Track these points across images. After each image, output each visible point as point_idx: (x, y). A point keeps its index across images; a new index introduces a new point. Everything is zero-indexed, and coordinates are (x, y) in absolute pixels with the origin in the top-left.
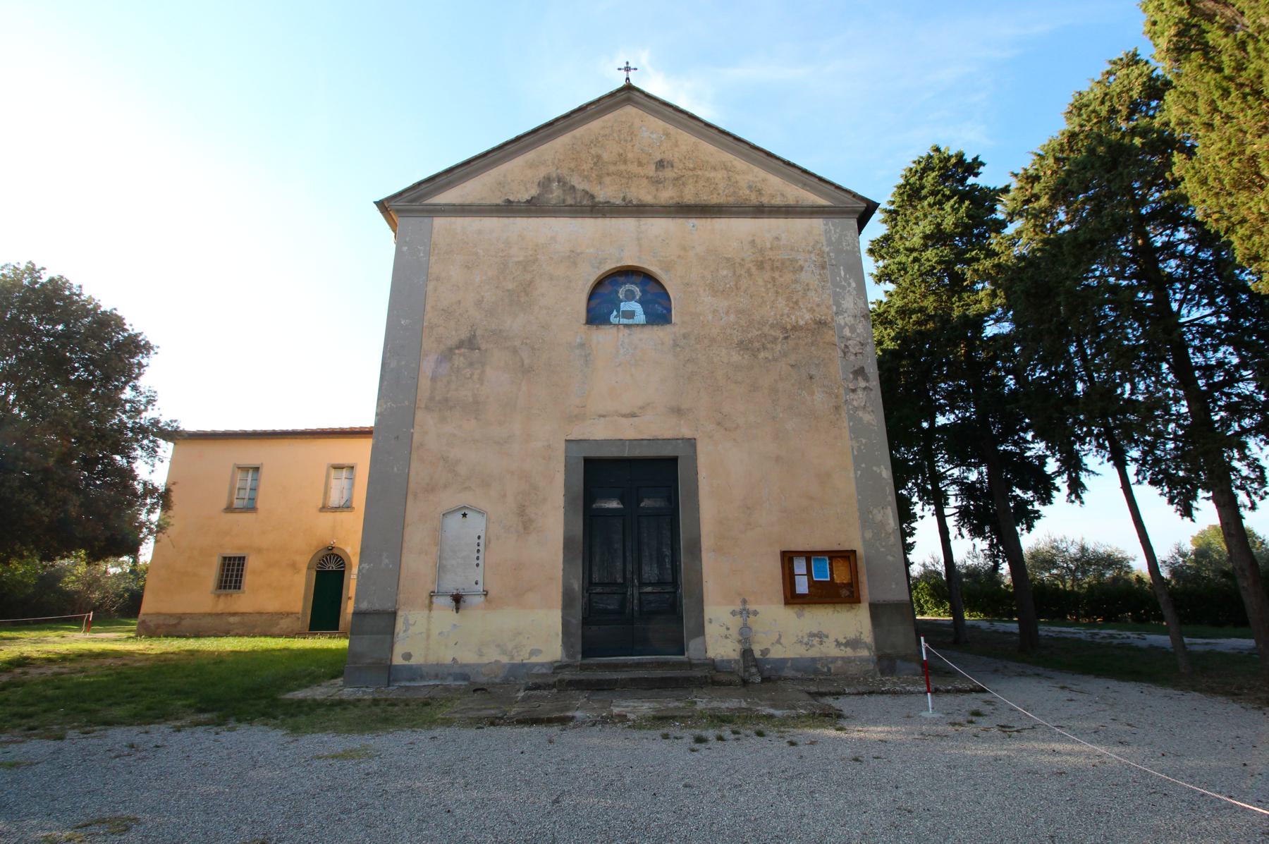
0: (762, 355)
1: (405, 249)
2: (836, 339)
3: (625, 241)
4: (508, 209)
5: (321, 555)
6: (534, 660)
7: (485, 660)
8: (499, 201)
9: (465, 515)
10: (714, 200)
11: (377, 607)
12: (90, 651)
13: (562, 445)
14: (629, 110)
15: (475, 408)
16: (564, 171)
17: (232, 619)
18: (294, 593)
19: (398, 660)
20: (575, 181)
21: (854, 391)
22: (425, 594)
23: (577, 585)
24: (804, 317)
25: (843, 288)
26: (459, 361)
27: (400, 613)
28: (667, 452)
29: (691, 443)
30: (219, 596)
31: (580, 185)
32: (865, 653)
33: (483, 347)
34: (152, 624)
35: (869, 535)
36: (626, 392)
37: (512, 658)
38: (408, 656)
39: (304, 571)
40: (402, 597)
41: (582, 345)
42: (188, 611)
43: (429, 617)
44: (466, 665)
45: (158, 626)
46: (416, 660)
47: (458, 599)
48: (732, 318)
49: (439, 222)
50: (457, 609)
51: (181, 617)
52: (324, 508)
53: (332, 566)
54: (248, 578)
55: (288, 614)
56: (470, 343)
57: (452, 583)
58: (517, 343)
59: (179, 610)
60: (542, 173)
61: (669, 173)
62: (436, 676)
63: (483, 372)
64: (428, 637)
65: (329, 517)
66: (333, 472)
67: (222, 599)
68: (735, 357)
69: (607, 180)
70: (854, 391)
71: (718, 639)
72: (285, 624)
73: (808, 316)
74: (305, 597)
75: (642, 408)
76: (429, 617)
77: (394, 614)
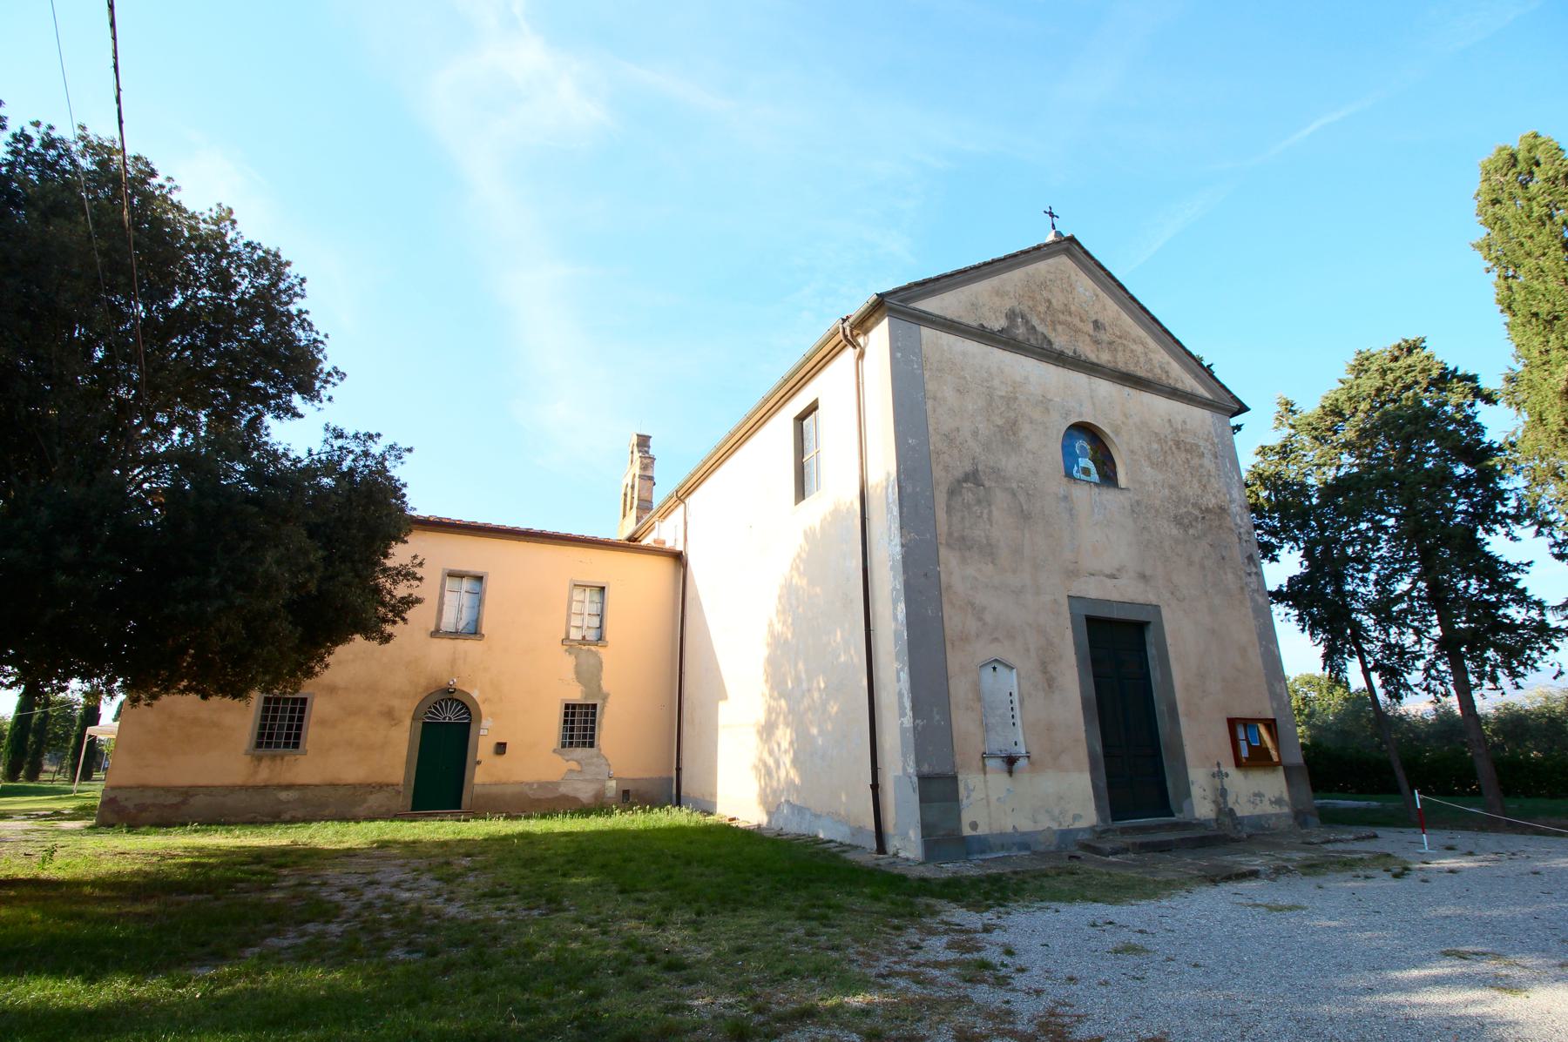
0: (1191, 531)
4: (983, 335)
5: (436, 698)
8: (975, 324)
10: (1141, 373)
11: (938, 770)
12: (218, 848)
13: (1065, 602)
14: (1063, 261)
15: (988, 551)
16: (1026, 310)
17: (283, 795)
18: (393, 756)
19: (967, 831)
20: (1035, 321)
22: (979, 756)
23: (1099, 748)
24: (1212, 502)
26: (969, 497)
28: (1142, 618)
30: (260, 759)
31: (1040, 328)
32: (1286, 810)
33: (987, 484)
34: (130, 805)
36: (1106, 550)
38: (974, 826)
39: (408, 722)
40: (958, 759)
41: (1066, 498)
42: (202, 781)
43: (986, 782)
45: (142, 808)
46: (982, 830)
47: (1011, 761)
48: (1167, 492)
49: (927, 333)
50: (1010, 773)
51: (188, 792)
52: (436, 633)
53: (449, 716)
55: (381, 786)
56: (973, 477)
58: (1014, 485)
60: (1008, 304)
61: (1105, 337)
62: (1003, 847)
63: (990, 512)
65: (446, 644)
66: (449, 583)
67: (265, 764)
68: (1175, 532)
69: (1060, 328)
71: (1202, 808)
72: (374, 800)
74: (408, 762)
76: (986, 782)
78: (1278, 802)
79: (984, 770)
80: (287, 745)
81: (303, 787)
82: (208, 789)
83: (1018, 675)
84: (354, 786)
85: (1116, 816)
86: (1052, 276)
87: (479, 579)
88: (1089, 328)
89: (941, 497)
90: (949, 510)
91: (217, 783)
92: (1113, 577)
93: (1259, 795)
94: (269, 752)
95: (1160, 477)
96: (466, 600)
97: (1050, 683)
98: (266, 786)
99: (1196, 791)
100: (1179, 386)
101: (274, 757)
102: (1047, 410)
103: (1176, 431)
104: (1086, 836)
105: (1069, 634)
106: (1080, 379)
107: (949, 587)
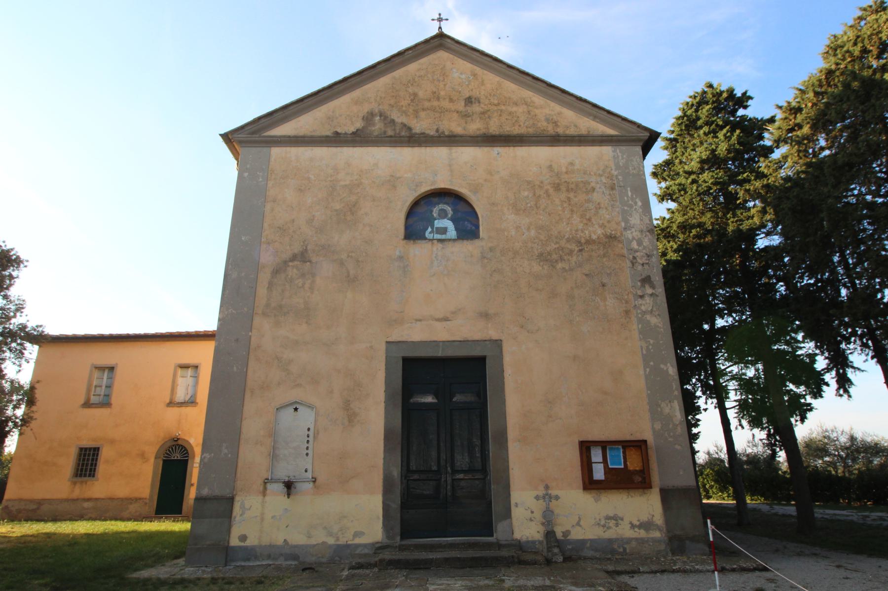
0: (560, 265)
1: (246, 174)
2: (625, 251)
3: (438, 167)
4: (337, 140)
5: (169, 444)
6: (358, 541)
7: (313, 542)
9: (296, 409)
11: (217, 492)
13: (383, 347)
16: (385, 108)
18: (143, 480)
19: (234, 542)
21: (642, 297)
22: (260, 482)
23: (396, 473)
24: (597, 232)
25: (631, 206)
26: (292, 272)
27: (237, 498)
28: (477, 352)
29: (497, 344)
30: (75, 483)
32: (657, 534)
33: (314, 259)
35: (658, 426)
36: (440, 298)
37: (338, 539)
38: (243, 538)
39: (152, 460)
40: (239, 484)
41: (401, 258)
42: (48, 496)
43: (263, 503)
44: (296, 546)
45: (19, 511)
46: (251, 541)
47: (289, 486)
49: (276, 151)
50: (289, 495)
51: (40, 503)
52: (171, 404)
53: (177, 456)
54: (101, 468)
55: (137, 500)
56: (302, 257)
57: (284, 471)
58: (344, 256)
59: (39, 495)
60: (366, 108)
62: (269, 557)
63: (313, 282)
64: (262, 519)
65: (176, 410)
69: (422, 114)
70: (642, 297)
72: (133, 508)
73: (600, 232)
75: (453, 313)
76: (263, 503)
77: (231, 500)
78: (647, 525)
79: (264, 493)
80: (90, 476)
81: (96, 499)
82: (50, 501)
83: (317, 414)
84: (122, 499)
85: (404, 535)
86: (422, 73)
87: (196, 367)
88: (461, 106)
89: (265, 277)
90: (271, 286)
91: (54, 497)
92: (446, 319)
93: (616, 519)
94: (79, 479)
95: (527, 220)
96: (190, 381)
97: (351, 417)
98: (77, 499)
99: (518, 514)
100: (572, 131)
101: (82, 482)
102: (395, 187)
103: (558, 174)
104: (366, 551)
105: (381, 376)
106: (440, 153)
107: (259, 347)
